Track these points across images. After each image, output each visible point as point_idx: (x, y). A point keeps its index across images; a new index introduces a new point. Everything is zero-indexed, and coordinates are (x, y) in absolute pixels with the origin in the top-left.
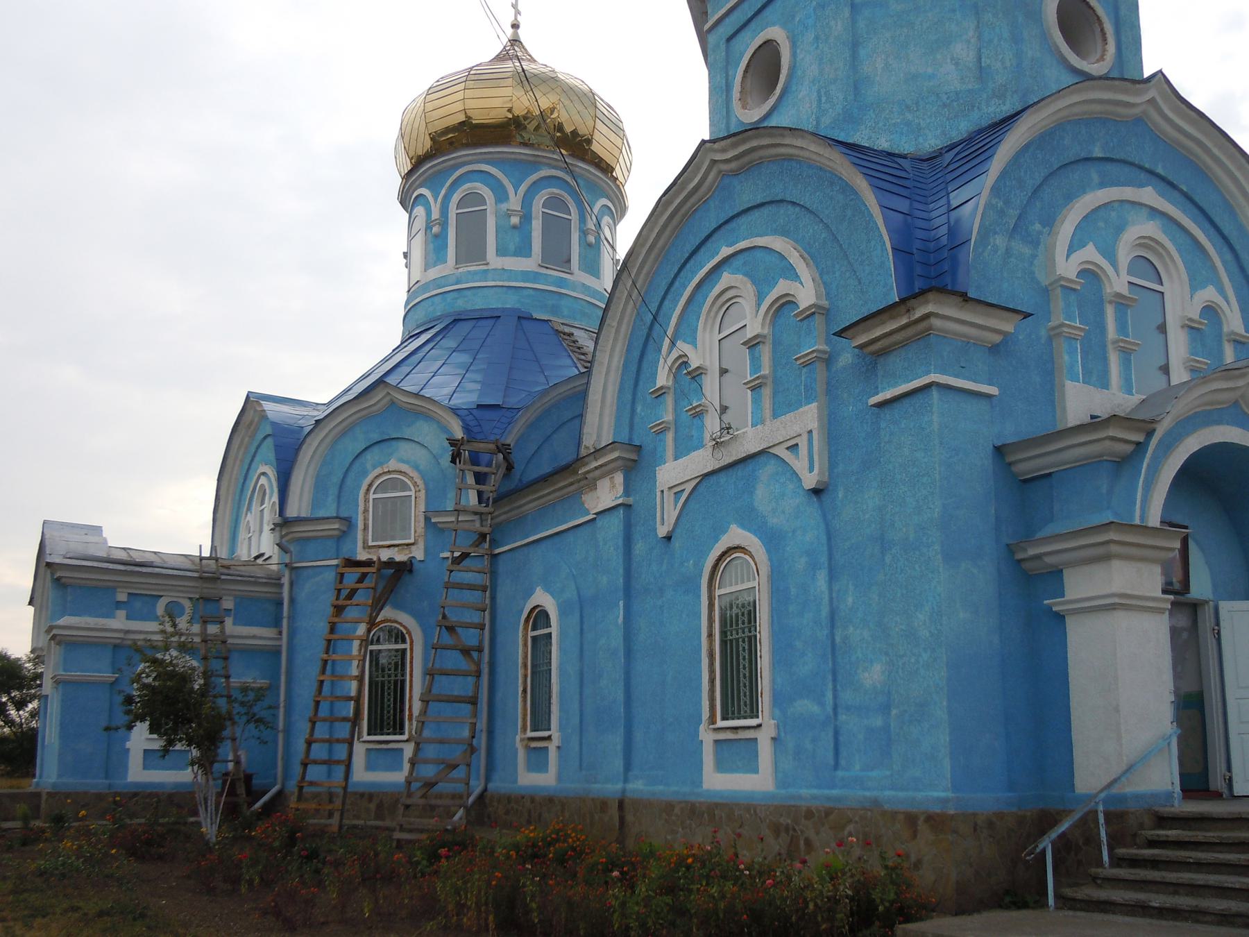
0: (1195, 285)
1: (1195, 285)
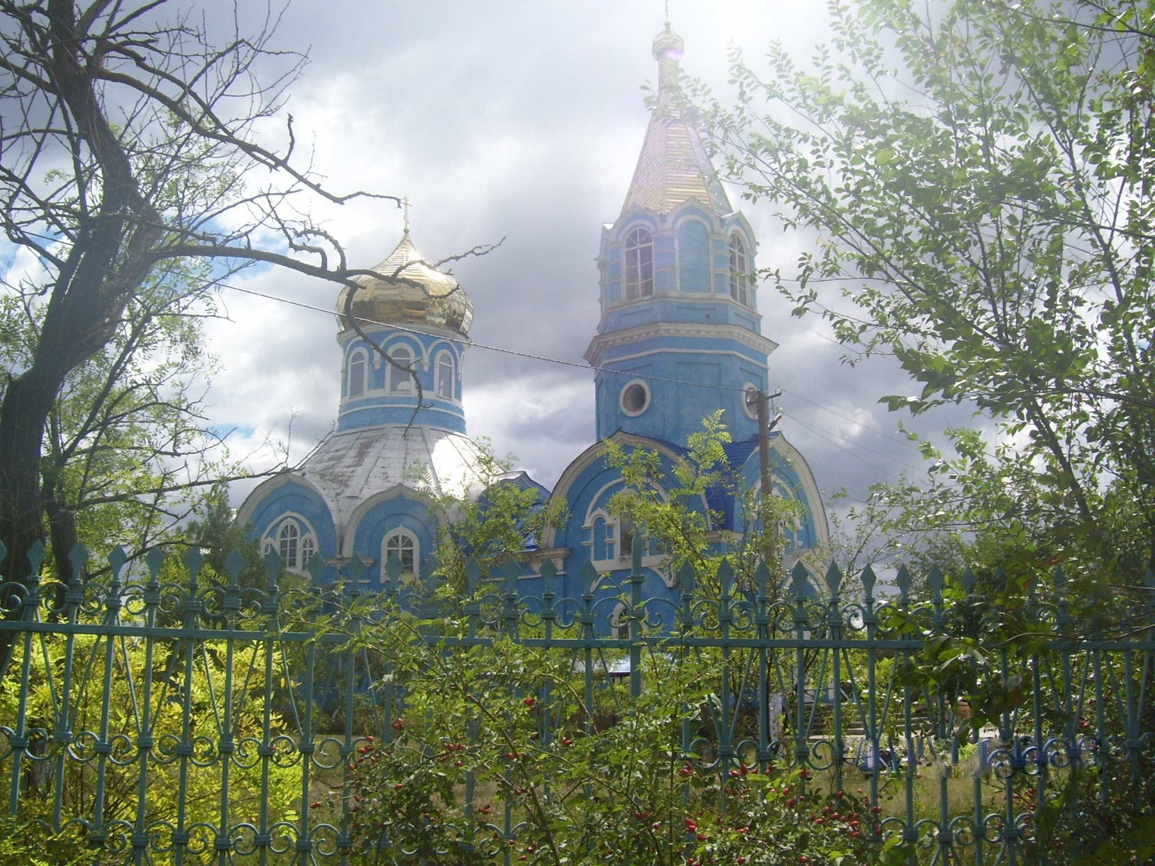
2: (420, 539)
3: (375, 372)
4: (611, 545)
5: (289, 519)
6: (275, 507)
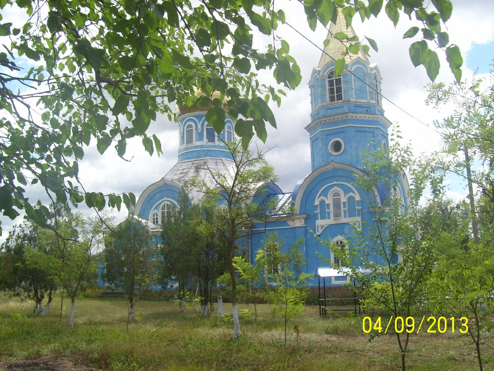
3: (199, 133)
4: (329, 213)
5: (166, 201)
6: (157, 196)
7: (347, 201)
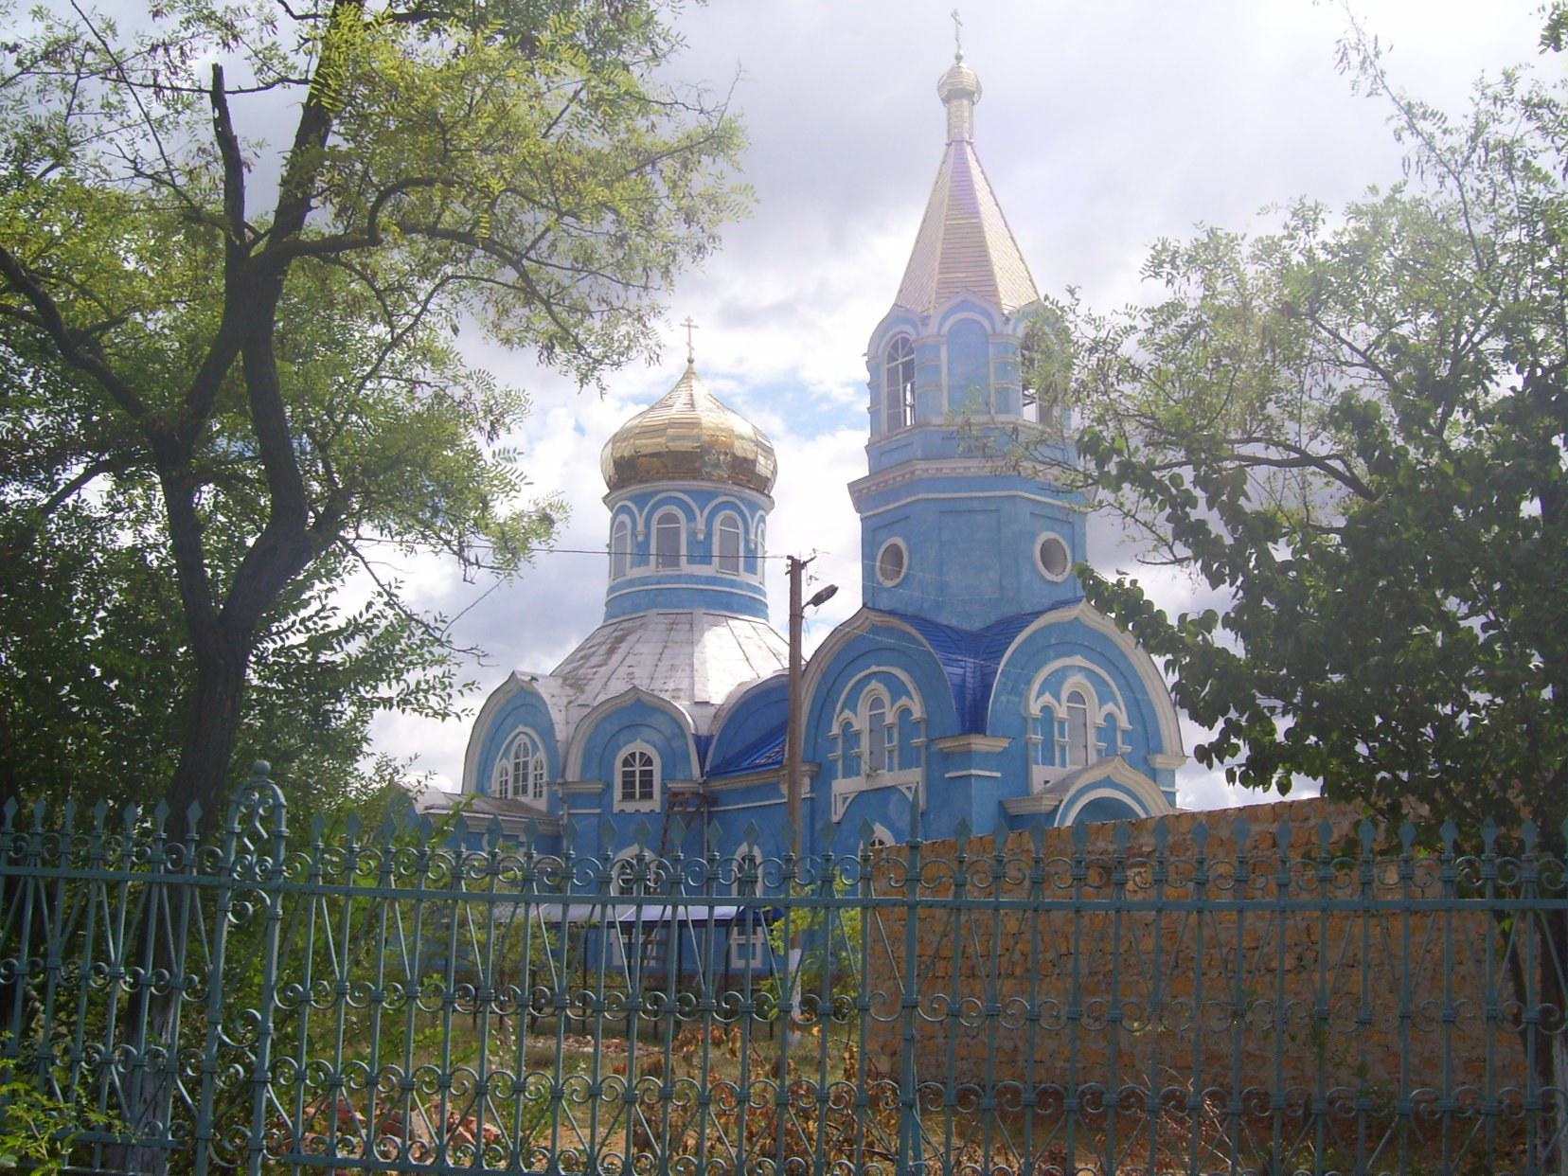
0: (1102, 702)
1: (1102, 702)
2: (662, 758)
3: (639, 545)
7: (896, 721)
